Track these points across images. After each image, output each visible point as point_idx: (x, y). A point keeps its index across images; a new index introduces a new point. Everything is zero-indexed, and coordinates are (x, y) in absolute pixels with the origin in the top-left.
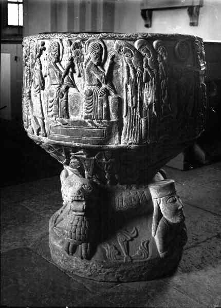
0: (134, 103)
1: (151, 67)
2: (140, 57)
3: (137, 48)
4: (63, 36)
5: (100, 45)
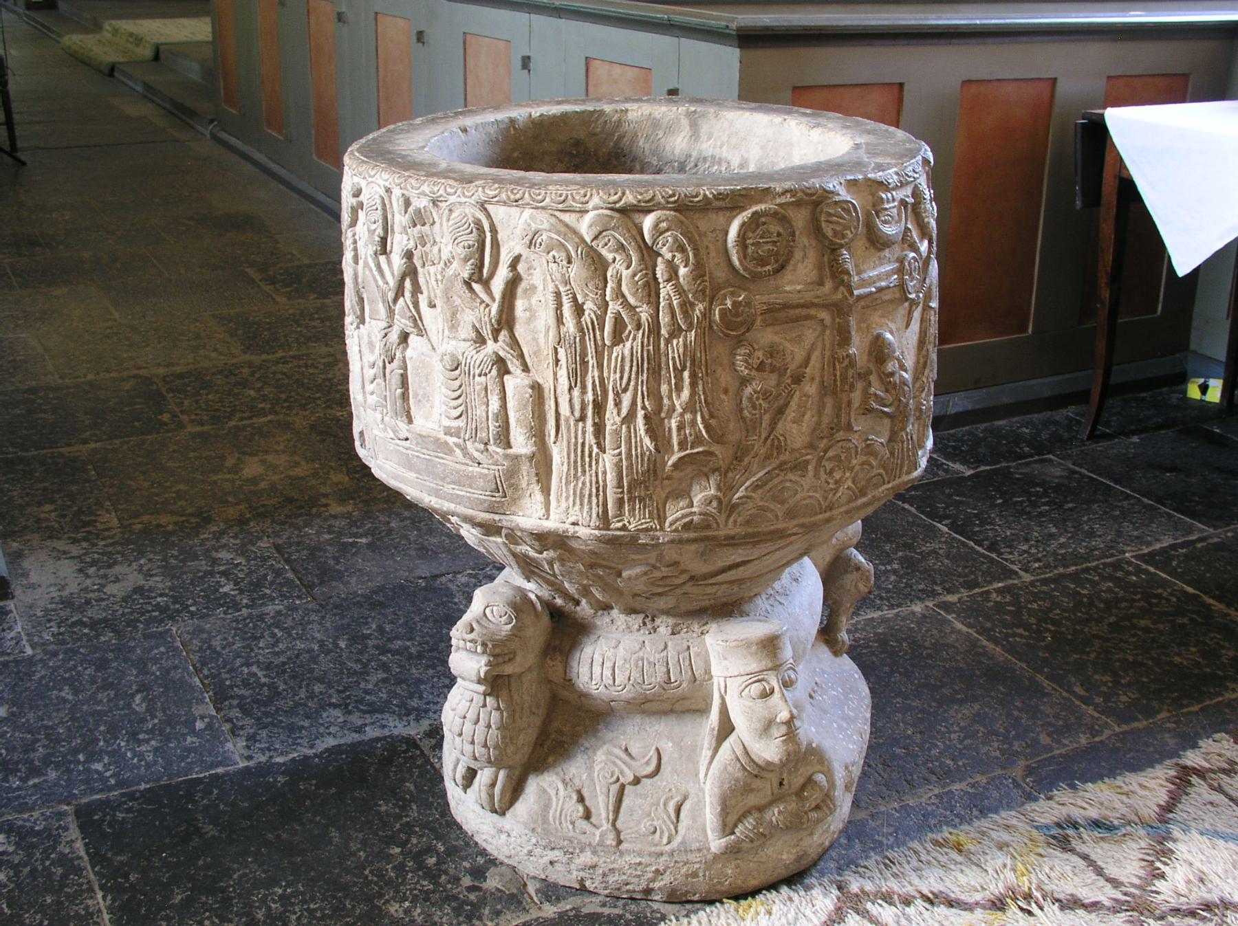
0: (577, 407)
1: (632, 300)
2: (598, 266)
3: (588, 240)
4: (391, 179)
5: (478, 223)
